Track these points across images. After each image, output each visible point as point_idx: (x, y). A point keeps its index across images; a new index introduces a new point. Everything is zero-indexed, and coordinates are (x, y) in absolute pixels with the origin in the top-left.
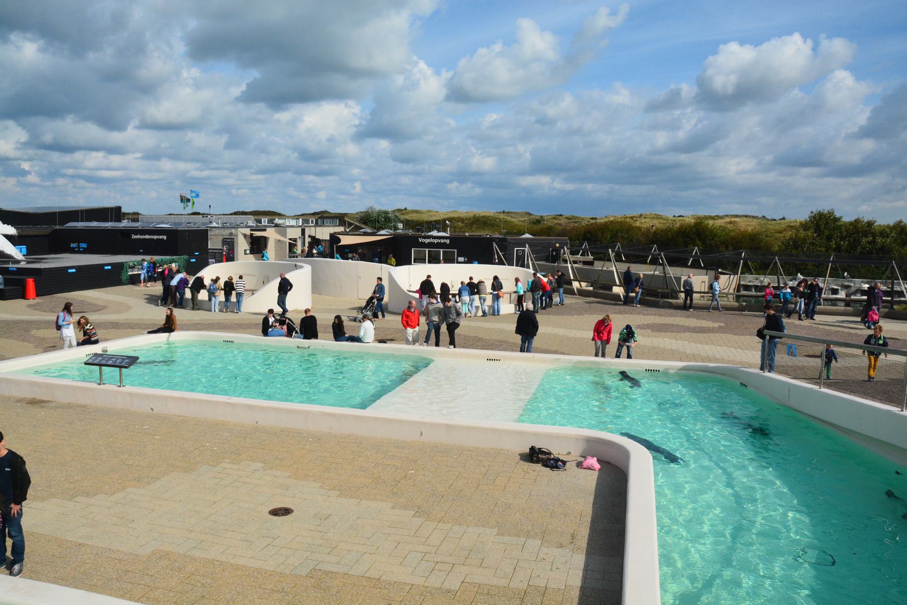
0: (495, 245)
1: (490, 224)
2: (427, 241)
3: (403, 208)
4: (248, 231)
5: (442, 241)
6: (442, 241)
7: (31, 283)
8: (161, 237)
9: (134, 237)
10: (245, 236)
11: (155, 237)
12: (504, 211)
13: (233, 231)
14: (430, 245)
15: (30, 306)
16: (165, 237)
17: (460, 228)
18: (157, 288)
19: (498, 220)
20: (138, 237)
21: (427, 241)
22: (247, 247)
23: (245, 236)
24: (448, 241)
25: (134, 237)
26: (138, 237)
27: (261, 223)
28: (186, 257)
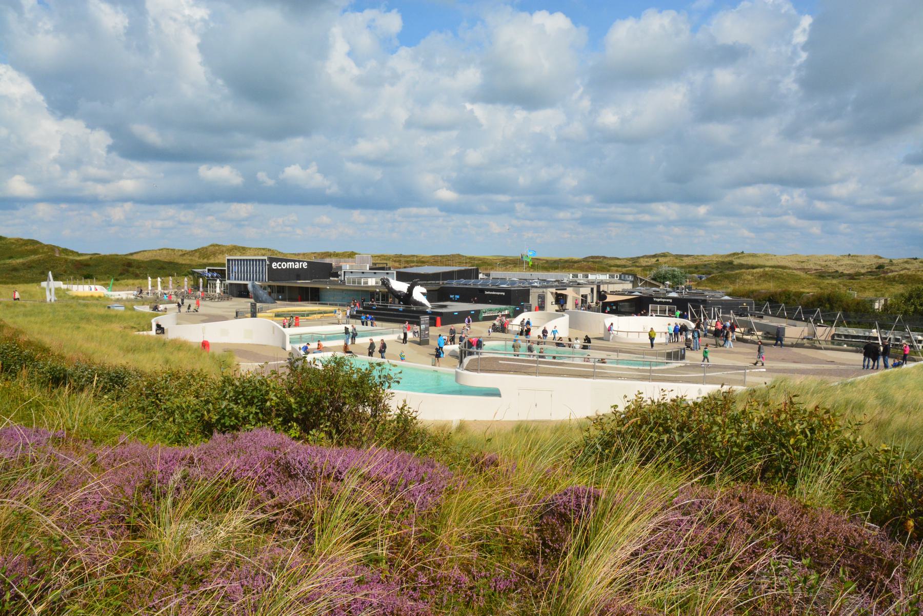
0: (689, 305)
1: (776, 277)
2: (658, 300)
3: (740, 252)
4: (554, 290)
5: (668, 300)
6: (668, 300)
7: (439, 319)
8: (501, 293)
9: (486, 293)
10: (552, 293)
11: (498, 293)
12: (849, 255)
13: (545, 290)
14: (660, 303)
15: (439, 330)
16: (504, 294)
17: (748, 281)
18: (368, 482)
19: (785, 274)
20: (489, 293)
21: (658, 300)
22: (553, 300)
23: (552, 293)
24: (671, 301)
25: (486, 293)
26: (489, 293)
27: (577, 277)
28: (514, 307)
